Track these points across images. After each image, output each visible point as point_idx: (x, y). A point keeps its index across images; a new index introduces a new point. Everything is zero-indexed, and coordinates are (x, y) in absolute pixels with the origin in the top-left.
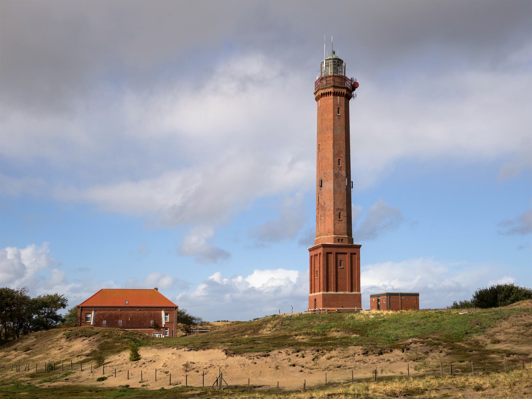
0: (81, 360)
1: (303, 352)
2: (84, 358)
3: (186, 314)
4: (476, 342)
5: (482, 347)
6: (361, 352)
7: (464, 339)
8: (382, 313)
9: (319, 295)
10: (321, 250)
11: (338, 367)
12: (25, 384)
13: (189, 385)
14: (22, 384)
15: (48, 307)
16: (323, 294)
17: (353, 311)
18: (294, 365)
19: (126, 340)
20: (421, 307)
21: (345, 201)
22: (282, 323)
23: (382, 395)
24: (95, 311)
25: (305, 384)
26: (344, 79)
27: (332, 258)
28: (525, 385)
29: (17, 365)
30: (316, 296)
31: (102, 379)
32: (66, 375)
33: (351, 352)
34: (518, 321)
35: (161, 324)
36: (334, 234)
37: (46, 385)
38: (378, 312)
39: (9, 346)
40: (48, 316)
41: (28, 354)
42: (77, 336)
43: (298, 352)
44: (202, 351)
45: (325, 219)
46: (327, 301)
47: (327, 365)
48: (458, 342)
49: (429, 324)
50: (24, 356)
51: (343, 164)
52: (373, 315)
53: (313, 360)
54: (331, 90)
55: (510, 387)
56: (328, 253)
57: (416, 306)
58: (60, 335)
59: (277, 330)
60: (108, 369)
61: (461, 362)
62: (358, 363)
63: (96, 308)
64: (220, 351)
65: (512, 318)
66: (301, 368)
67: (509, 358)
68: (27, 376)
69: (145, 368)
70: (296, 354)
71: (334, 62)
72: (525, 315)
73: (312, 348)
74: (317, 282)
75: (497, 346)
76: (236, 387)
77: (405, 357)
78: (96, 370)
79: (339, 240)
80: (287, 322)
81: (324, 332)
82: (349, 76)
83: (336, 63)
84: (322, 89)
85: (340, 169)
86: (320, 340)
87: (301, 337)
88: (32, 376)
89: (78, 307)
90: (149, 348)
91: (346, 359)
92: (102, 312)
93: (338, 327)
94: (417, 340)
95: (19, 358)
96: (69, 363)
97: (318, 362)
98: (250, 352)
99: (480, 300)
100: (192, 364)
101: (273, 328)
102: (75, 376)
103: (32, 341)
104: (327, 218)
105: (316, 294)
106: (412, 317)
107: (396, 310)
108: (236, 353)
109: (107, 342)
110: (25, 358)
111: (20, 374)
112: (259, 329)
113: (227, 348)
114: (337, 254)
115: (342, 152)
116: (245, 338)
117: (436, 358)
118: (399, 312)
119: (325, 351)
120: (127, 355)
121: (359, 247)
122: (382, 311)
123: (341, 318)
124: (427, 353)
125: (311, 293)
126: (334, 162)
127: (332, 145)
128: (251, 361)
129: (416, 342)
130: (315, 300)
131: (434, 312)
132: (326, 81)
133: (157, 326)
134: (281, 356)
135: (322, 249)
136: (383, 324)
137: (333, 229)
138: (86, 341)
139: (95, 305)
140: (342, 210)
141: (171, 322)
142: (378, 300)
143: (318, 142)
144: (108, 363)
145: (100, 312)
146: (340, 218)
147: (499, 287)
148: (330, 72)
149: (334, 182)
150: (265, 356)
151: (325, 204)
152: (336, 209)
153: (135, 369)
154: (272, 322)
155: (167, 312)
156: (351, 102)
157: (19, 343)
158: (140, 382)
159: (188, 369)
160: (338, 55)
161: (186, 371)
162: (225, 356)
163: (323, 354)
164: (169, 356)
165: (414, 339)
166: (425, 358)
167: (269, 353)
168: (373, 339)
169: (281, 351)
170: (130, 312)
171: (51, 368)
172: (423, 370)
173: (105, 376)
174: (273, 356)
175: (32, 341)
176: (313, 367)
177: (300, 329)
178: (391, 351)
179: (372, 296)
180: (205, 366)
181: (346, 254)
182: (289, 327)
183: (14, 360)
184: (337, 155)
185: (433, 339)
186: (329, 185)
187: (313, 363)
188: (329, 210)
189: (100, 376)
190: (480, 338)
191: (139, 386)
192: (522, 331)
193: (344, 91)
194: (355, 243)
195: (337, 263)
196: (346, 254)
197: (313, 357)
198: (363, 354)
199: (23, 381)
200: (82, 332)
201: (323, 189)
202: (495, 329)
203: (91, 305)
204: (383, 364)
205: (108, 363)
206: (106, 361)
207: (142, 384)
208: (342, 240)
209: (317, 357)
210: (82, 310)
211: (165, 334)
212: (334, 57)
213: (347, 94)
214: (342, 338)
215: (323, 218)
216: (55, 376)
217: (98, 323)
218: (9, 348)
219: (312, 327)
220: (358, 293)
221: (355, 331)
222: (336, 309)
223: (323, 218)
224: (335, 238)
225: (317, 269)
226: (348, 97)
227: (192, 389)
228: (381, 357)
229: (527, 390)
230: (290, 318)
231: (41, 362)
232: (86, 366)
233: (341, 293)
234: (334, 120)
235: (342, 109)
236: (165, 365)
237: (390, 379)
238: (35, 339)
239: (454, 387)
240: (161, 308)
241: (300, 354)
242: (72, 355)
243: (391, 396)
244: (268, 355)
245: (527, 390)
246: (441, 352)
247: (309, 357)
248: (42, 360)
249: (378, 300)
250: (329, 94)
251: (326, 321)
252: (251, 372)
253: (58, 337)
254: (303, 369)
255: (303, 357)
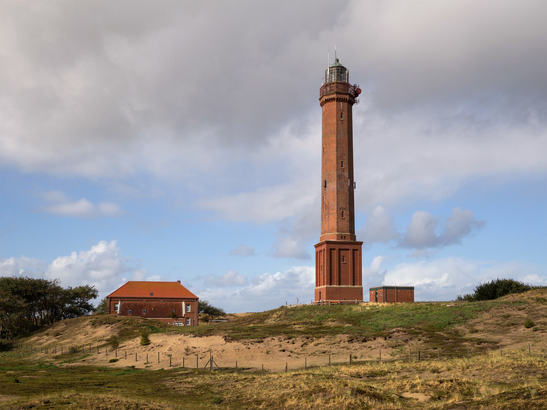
0: (102, 344)
1: (294, 339)
2: (104, 342)
3: (208, 305)
4: (456, 332)
5: (460, 336)
6: (346, 339)
7: (445, 329)
8: (378, 305)
9: (323, 288)
10: (324, 247)
11: (323, 353)
12: (48, 364)
13: (199, 367)
14: (46, 364)
15: (80, 297)
16: (327, 288)
17: (353, 303)
18: (284, 351)
19: (144, 327)
20: (416, 299)
21: (348, 201)
22: (286, 313)
23: (346, 376)
24: (122, 301)
25: (286, 367)
26: (347, 85)
27: (335, 254)
28: (475, 368)
29: (46, 348)
30: (321, 289)
31: (114, 361)
32: (84, 357)
33: (338, 339)
34: (498, 313)
35: (182, 314)
36: (338, 232)
37: (65, 365)
38: (375, 304)
39: (42, 332)
40: (80, 306)
41: (57, 339)
42: (101, 323)
43: (290, 339)
44: (205, 338)
45: (329, 217)
46: (330, 294)
47: (314, 351)
48: (439, 331)
49: (417, 315)
50: (54, 340)
51: (346, 166)
52: (370, 307)
53: (302, 346)
54: (334, 96)
55: (463, 370)
56: (331, 249)
57: (411, 299)
58: (87, 322)
59: (281, 320)
60: (121, 352)
61: (435, 349)
62: (342, 349)
63: (122, 299)
64: (221, 337)
65: (493, 311)
66: (289, 353)
67: (479, 346)
68: (53, 358)
69: (153, 352)
70: (287, 341)
71: (338, 69)
72: (505, 308)
73: (303, 335)
74: (322, 276)
75: (475, 336)
76: (227, 368)
77: (386, 345)
78: (110, 353)
79: (342, 237)
80: (292, 312)
81: (321, 322)
82: (352, 82)
83: (340, 71)
84: (326, 95)
85: (343, 171)
86: (316, 329)
87: (298, 326)
88: (57, 358)
89: (108, 297)
90: (160, 334)
91: (332, 346)
92: (128, 302)
93: (333, 317)
94: (401, 329)
95: (49, 342)
96: (88, 347)
97: (306, 348)
98: (246, 338)
99: (481, 294)
100: (193, 349)
101: (277, 318)
102: (92, 358)
103: (62, 327)
104: (331, 216)
105: (321, 287)
106: (405, 309)
107: (391, 303)
108: (233, 339)
109: (127, 329)
110: (54, 342)
111: (48, 356)
112: (265, 319)
113: (226, 335)
114: (340, 250)
115: (344, 155)
116: (250, 328)
117: (415, 344)
118: (393, 304)
119: (314, 338)
120: (138, 340)
121: (361, 243)
122: (378, 303)
123: (340, 310)
124: (406, 341)
125: (317, 286)
126: (337, 164)
127: (335, 148)
128: (246, 346)
129: (399, 331)
130: (320, 293)
131: (424, 304)
132: (330, 88)
133: (176, 316)
134: (273, 342)
135: (325, 245)
136: (376, 315)
137: (336, 227)
138: (109, 328)
139: (122, 296)
140: (345, 209)
141: (192, 312)
142: (376, 293)
143: (322, 145)
144: (122, 347)
145: (126, 302)
146: (343, 216)
147: (499, 282)
148: (334, 79)
149: (337, 183)
150: (259, 342)
151: (329, 204)
152: (338, 208)
153: (143, 352)
154: (278, 312)
155: (188, 303)
156: (354, 107)
157: (51, 329)
158: (145, 364)
159: (188, 353)
160: (342, 63)
161: (187, 355)
162: (224, 342)
163: (312, 341)
164: (175, 341)
165: (399, 329)
166: (403, 345)
167: (263, 340)
168: (361, 329)
169: (275, 338)
170: (154, 302)
171: (74, 351)
172: (398, 356)
173: (118, 358)
174: (266, 342)
175: (62, 327)
176: (301, 352)
177: (301, 319)
178: (375, 339)
179: (371, 290)
180: (204, 351)
181: (348, 250)
182: (292, 317)
183: (45, 344)
184: (340, 157)
185: (416, 329)
186: (333, 186)
187: (301, 349)
188: (333, 209)
189: (113, 357)
190: (460, 328)
191: (144, 367)
192: (499, 322)
193: (347, 97)
194: (358, 239)
195: (340, 257)
196: (348, 250)
197: (302, 343)
198: (349, 341)
199: (47, 362)
200: (106, 320)
201: (327, 189)
202: (477, 320)
203: (119, 296)
204: (365, 350)
205: (122, 347)
206: (120, 345)
207: (146, 365)
208: (345, 237)
209: (306, 344)
210: (111, 301)
211: (186, 323)
212: (338, 65)
213: (349, 100)
214: (336, 327)
215: (327, 217)
216: (75, 357)
217: (123, 312)
218: (42, 333)
219: (312, 317)
220: (360, 286)
221: (348, 321)
222: (339, 301)
223: (327, 217)
224: (338, 235)
225: (322, 264)
226: (351, 102)
227: (186, 369)
228: (364, 344)
229: (476, 372)
230: (294, 309)
231: (68, 346)
232: (104, 350)
233: (344, 286)
234: (337, 124)
235: (345, 114)
236: (170, 350)
237: (363, 363)
238: (65, 326)
239: (415, 370)
240: (182, 299)
241: (291, 341)
242: (95, 340)
243: (354, 377)
244: (262, 342)
245: (476, 372)
246: (420, 340)
247: (299, 343)
248: (67, 343)
249: (376, 293)
250: (333, 99)
251: (326, 312)
252: (243, 356)
253: (84, 324)
254: (291, 354)
255: (293, 343)
